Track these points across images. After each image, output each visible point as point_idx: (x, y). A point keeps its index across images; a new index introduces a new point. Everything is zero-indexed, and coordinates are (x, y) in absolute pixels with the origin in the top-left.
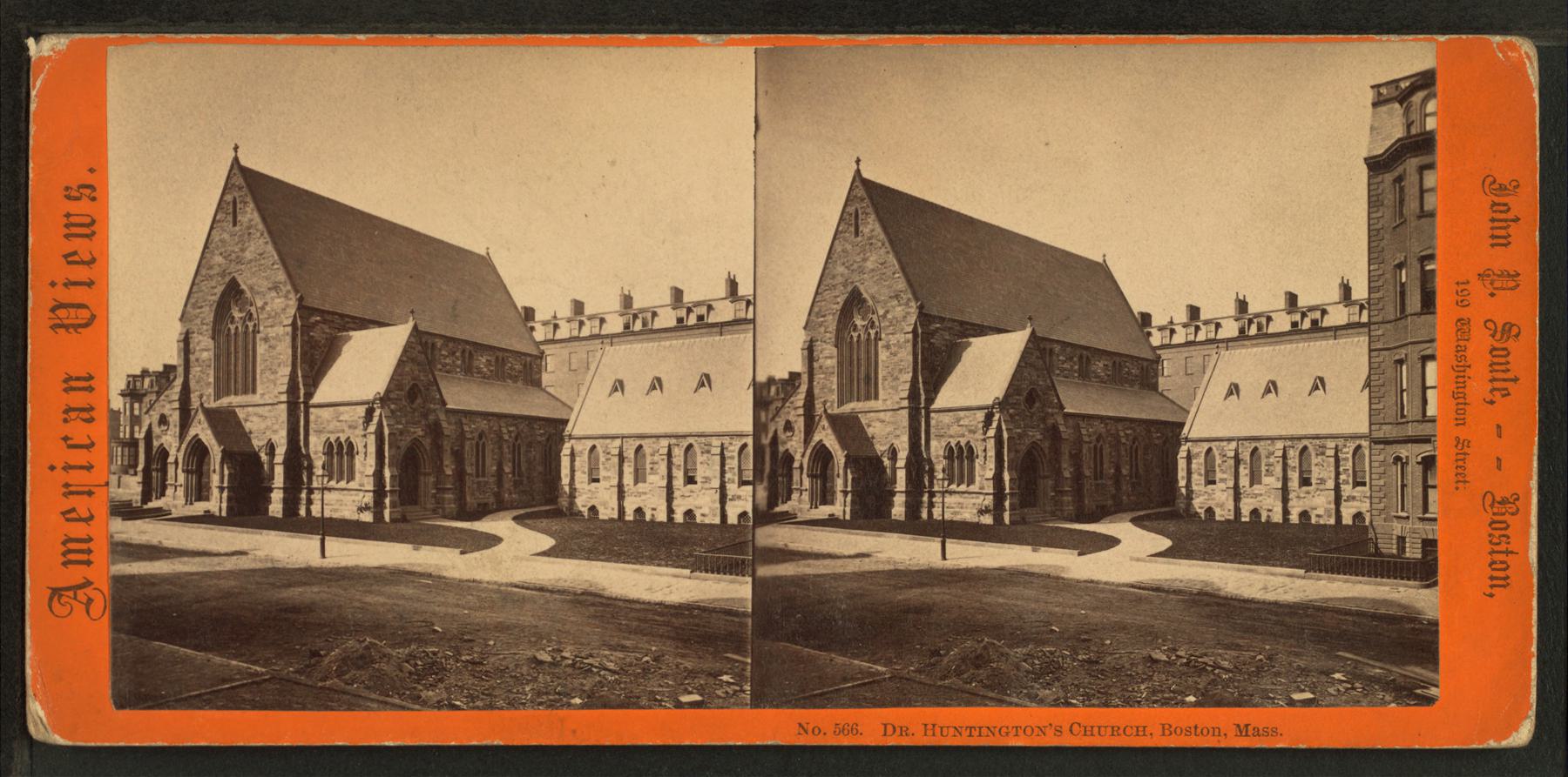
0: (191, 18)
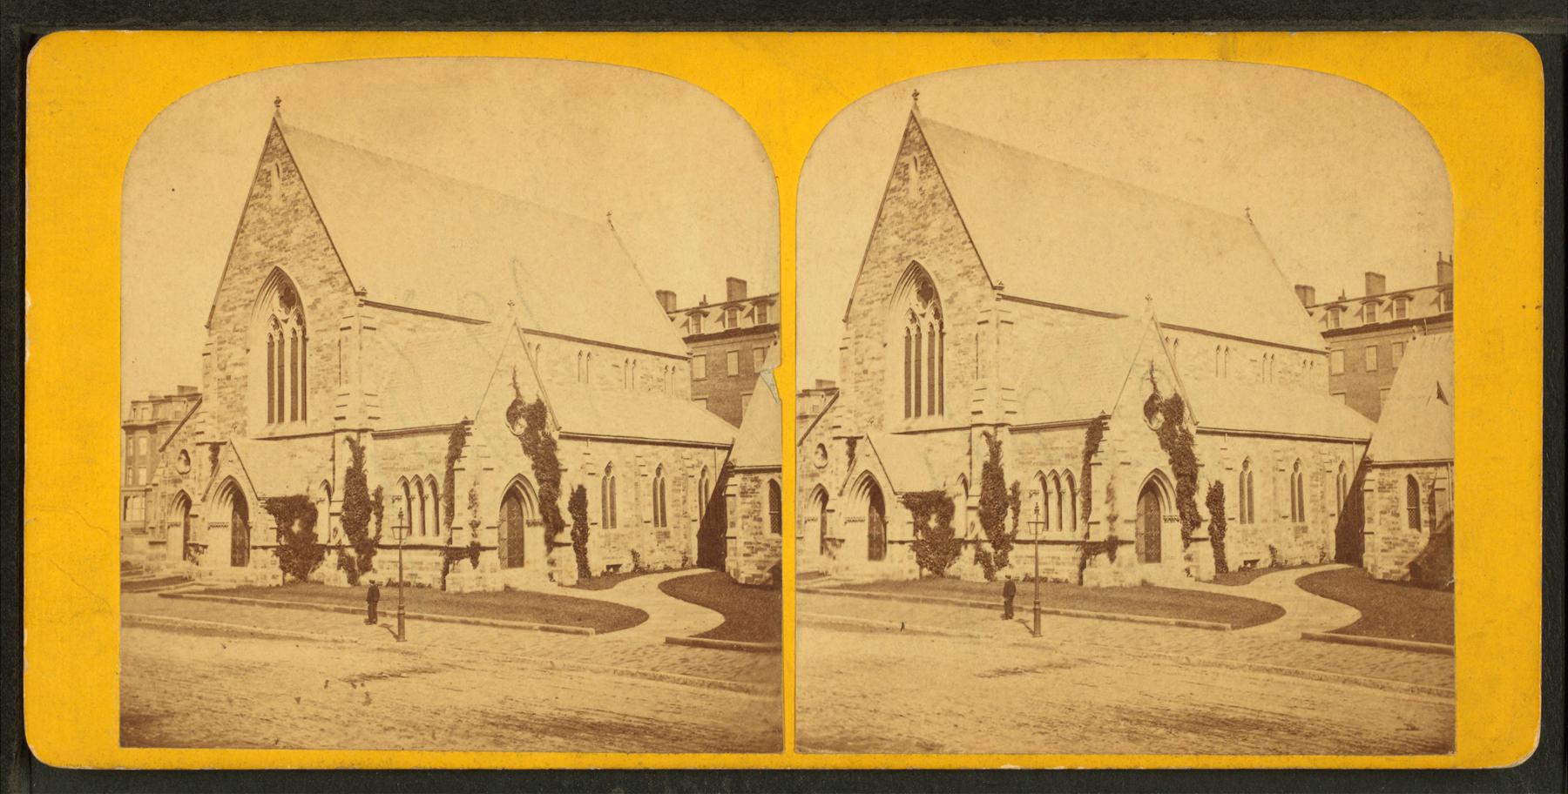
0: (184, 18)
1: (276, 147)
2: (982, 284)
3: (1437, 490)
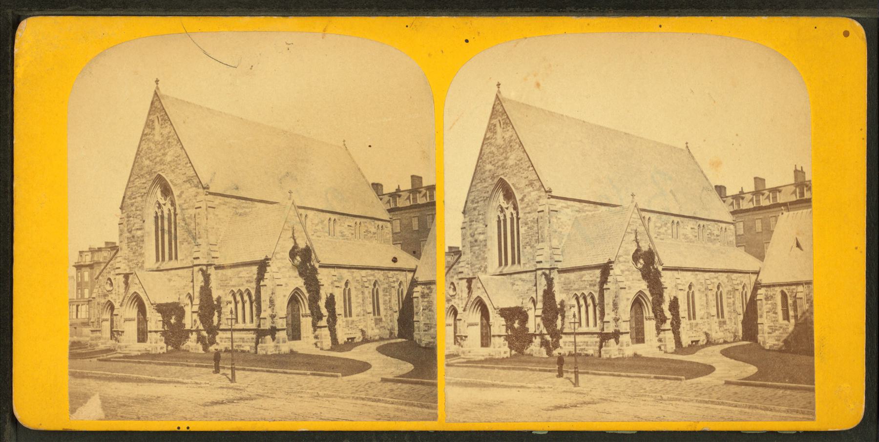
1: (157, 106)
2: (539, 190)
3: (798, 298)
